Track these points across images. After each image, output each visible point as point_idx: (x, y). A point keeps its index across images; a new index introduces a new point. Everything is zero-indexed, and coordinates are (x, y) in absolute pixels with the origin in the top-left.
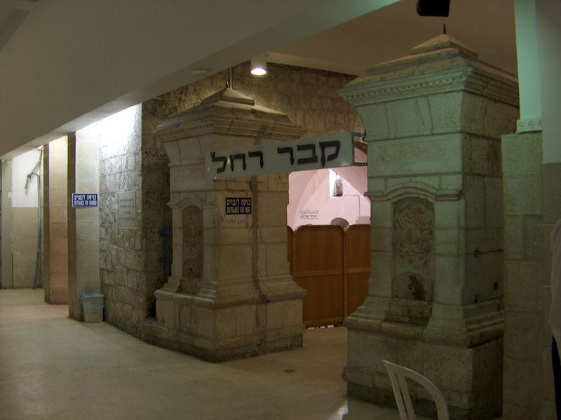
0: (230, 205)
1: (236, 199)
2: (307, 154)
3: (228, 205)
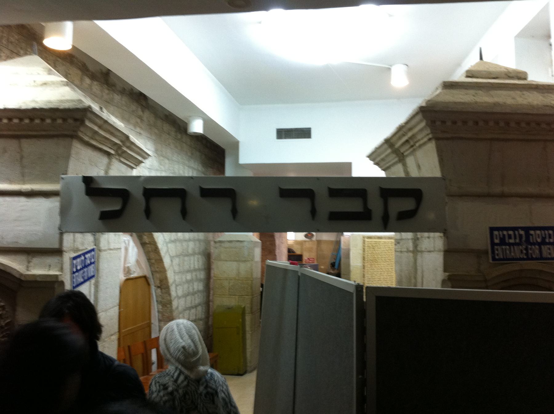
0: (503, 242)
1: (514, 229)
2: (354, 205)
3: (497, 241)
